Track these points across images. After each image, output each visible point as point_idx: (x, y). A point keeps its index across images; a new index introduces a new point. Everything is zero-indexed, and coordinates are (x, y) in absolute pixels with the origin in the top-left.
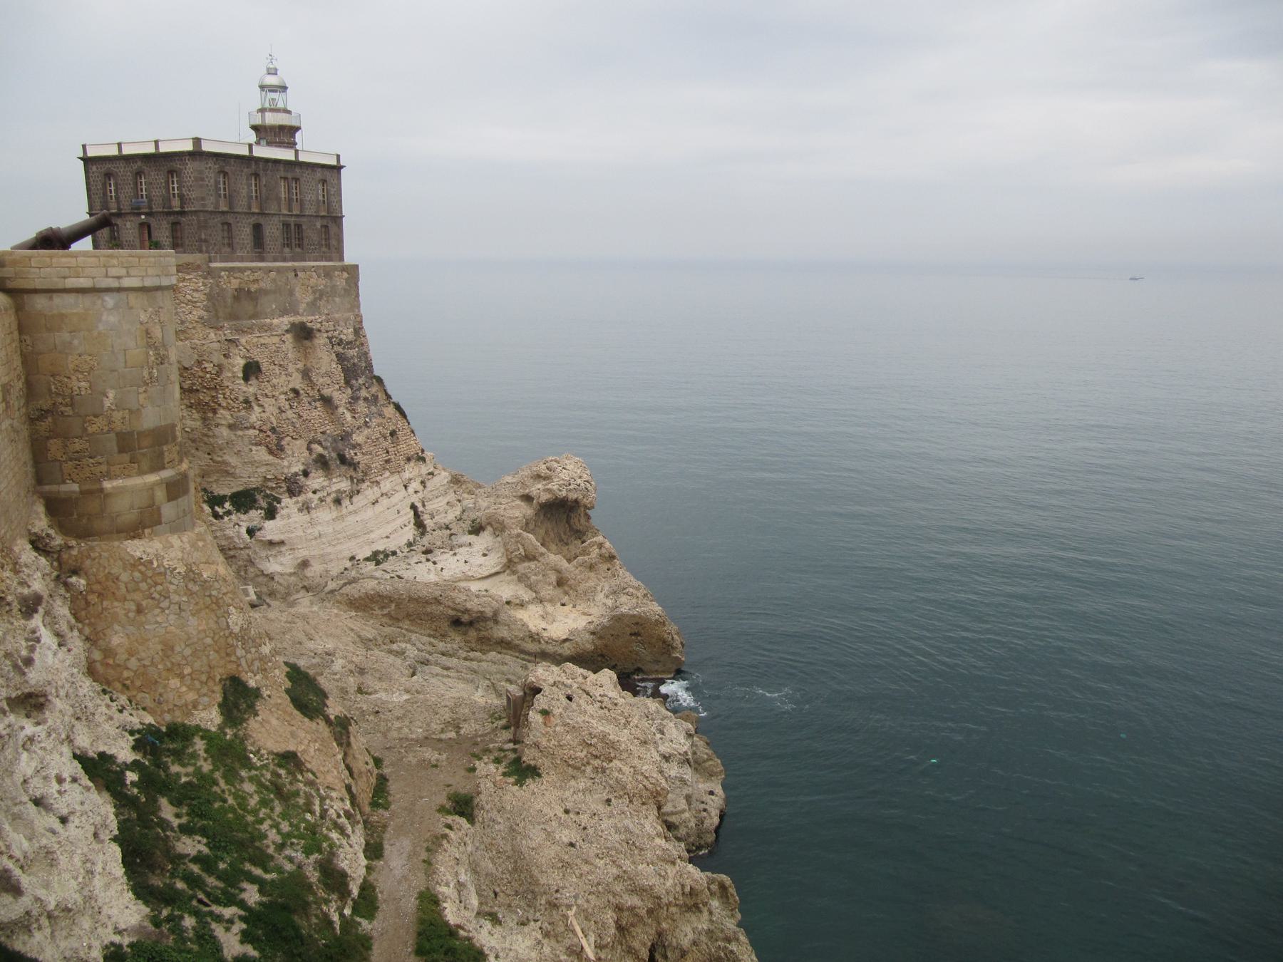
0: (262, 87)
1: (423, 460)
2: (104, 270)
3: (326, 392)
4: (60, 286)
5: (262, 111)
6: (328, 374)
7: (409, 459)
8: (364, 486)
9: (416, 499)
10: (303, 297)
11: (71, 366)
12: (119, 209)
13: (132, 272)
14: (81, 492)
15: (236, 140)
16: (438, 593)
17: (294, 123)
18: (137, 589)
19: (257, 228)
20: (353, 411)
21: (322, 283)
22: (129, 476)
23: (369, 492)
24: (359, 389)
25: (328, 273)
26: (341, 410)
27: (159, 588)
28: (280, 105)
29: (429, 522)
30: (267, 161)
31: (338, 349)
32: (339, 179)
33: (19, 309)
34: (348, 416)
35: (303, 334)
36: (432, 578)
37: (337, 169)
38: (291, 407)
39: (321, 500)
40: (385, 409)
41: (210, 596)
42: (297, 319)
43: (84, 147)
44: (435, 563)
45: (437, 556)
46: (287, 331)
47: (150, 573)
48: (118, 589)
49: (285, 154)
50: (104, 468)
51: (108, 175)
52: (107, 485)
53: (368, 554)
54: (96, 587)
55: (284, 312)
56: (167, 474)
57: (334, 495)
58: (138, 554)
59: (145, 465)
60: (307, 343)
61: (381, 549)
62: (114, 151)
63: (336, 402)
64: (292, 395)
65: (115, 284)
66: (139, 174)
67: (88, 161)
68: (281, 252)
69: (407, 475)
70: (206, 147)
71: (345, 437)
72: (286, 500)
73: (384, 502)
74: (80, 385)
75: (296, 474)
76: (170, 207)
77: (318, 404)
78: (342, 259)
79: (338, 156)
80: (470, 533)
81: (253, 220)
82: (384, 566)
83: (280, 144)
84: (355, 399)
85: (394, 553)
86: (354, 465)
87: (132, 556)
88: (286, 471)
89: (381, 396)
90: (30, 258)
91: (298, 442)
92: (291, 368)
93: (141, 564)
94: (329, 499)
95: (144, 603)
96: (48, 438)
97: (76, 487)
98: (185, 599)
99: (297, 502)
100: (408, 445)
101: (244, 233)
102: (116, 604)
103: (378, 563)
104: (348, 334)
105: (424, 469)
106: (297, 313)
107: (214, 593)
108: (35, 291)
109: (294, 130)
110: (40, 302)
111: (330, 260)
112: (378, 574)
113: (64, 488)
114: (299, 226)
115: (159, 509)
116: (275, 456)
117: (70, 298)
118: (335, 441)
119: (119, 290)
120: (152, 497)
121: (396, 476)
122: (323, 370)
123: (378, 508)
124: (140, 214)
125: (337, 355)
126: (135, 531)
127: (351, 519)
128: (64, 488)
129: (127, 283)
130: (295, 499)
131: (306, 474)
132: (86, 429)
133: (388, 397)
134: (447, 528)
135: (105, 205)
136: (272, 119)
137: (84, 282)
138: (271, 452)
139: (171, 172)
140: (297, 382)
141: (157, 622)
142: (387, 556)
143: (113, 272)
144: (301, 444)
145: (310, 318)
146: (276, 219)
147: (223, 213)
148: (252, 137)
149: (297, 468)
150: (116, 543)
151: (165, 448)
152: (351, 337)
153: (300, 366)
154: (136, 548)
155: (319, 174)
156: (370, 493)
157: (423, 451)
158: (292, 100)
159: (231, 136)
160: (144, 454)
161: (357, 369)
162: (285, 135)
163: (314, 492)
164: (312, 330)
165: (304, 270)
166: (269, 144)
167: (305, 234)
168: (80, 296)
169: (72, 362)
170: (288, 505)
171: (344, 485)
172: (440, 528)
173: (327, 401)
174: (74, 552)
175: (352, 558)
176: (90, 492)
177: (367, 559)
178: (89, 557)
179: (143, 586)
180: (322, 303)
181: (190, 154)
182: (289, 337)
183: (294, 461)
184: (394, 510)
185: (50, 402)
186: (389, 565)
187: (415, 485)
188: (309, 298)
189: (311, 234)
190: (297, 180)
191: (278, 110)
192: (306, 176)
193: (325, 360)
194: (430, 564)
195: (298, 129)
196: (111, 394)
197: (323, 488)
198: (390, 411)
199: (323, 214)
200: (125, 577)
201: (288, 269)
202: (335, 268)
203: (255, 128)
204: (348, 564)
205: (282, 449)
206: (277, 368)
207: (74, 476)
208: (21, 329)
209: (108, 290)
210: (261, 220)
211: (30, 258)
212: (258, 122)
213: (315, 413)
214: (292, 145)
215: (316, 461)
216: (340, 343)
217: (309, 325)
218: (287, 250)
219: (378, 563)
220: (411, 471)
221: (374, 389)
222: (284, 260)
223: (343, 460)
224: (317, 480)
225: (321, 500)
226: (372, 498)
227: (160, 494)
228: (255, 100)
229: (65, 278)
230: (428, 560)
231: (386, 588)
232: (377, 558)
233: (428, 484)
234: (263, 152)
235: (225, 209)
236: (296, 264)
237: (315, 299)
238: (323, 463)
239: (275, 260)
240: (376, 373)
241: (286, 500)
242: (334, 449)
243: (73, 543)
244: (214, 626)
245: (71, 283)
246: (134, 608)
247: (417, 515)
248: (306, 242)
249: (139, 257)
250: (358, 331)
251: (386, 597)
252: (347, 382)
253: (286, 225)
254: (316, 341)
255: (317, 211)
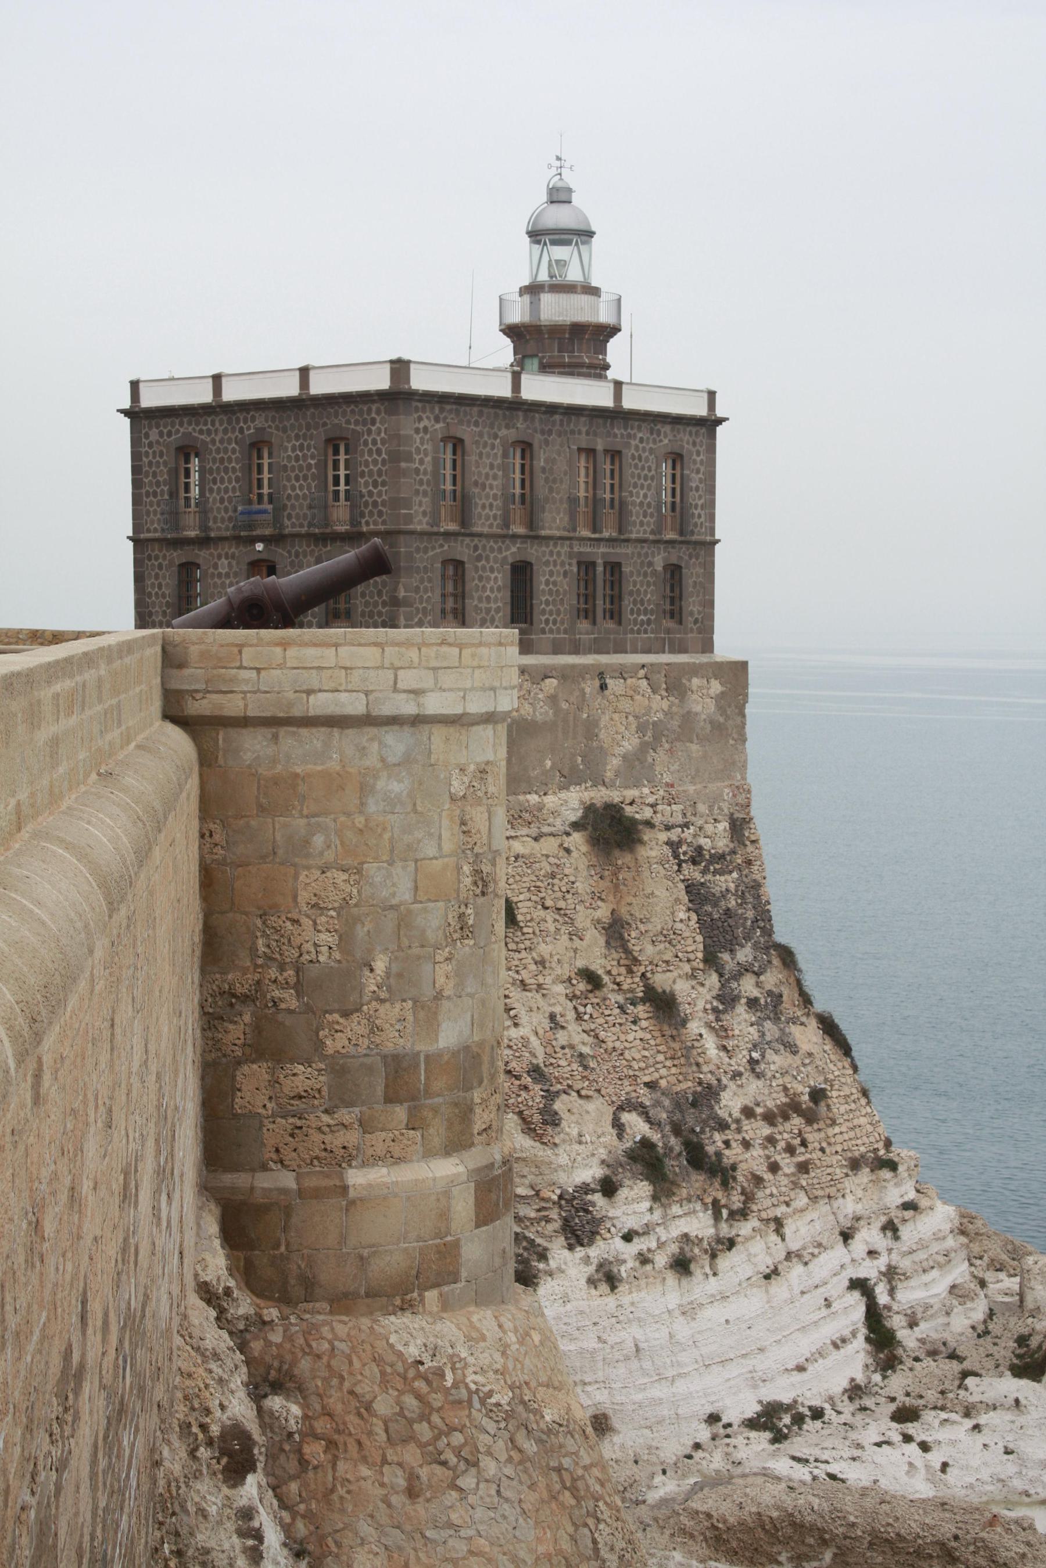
0: (536, 235)
1: (892, 1166)
2: (390, 675)
3: (661, 980)
4: (297, 712)
5: (533, 290)
6: (669, 936)
7: (855, 1165)
8: (745, 1228)
9: (869, 1270)
10: (620, 740)
11: (304, 896)
12: (204, 527)
13: (448, 679)
14: (301, 1193)
15: (465, 364)
16: (948, 1529)
17: (604, 316)
18: (410, 1438)
19: (521, 574)
20: (722, 1032)
21: (660, 704)
22: (399, 1160)
23: (757, 1246)
24: (737, 976)
25: (674, 684)
26: (695, 1027)
27: (457, 1439)
28: (574, 274)
29: (908, 1339)
30: (552, 409)
31: (692, 872)
32: (712, 449)
33: (206, 760)
34: (710, 1044)
35: (612, 832)
36: (921, 1488)
37: (710, 424)
38: (579, 1017)
39: (644, 1259)
40: (795, 1030)
41: (559, 1470)
42: (601, 795)
43: (135, 385)
44: (925, 1447)
45: (930, 1426)
46: (576, 826)
47: (437, 1400)
48: (370, 1433)
49: (591, 394)
50: (352, 1137)
51: (185, 451)
52: (357, 1178)
53: (752, 1409)
54: (322, 1425)
55: (570, 778)
56: (476, 1157)
57: (674, 1248)
58: (413, 1351)
59: (437, 1132)
60: (624, 859)
61: (786, 1398)
62: (204, 396)
63: (685, 1009)
64: (582, 986)
65: (409, 708)
66: (257, 446)
67: (136, 415)
68: (571, 630)
69: (849, 1206)
70: (420, 381)
71: (710, 1093)
72: (559, 1254)
73: (796, 1272)
74: (319, 942)
75: (585, 1189)
76: (327, 522)
77: (641, 1011)
78: (708, 646)
79: (712, 395)
80: (1020, 1371)
81: (512, 552)
82: (798, 1445)
83: (572, 369)
84: (727, 1000)
85: (817, 1414)
86: (721, 1172)
87: (400, 1355)
88: (562, 1178)
89: (789, 994)
90: (240, 647)
91: (591, 1106)
92: (583, 918)
93: (419, 1376)
94: (661, 1260)
95: (424, 1473)
96: (239, 1063)
97: (288, 1180)
98: (509, 1471)
99: (587, 1260)
100: (853, 1127)
101: (491, 585)
102: (365, 1471)
103: (779, 1438)
104: (716, 837)
105: (898, 1191)
106: (599, 781)
107: (566, 1462)
108: (244, 722)
109: (603, 334)
110: (253, 745)
111: (681, 648)
112: (782, 1466)
113: (264, 1181)
114: (614, 568)
115: (456, 1244)
116: (539, 1138)
117: (315, 738)
118: (677, 1105)
119: (418, 721)
120: (444, 1215)
121: (823, 1207)
122: (656, 925)
123: (779, 1289)
124: (253, 540)
125: (691, 888)
126: (401, 1294)
127: (714, 1314)
128: (264, 1181)
129: (434, 704)
130: (580, 1252)
131: (609, 1188)
132: (320, 1044)
133: (806, 1000)
134: (953, 1356)
135: (174, 517)
136: (555, 309)
137: (353, 705)
138: (529, 1128)
139: (333, 443)
140: (596, 955)
141: (450, 1525)
142: (799, 1420)
143: (408, 679)
144: (598, 1111)
145: (631, 793)
146: (564, 549)
147: (447, 535)
148: (503, 352)
149: (590, 1173)
150: (365, 1322)
151: (477, 1095)
152: (723, 844)
153: (603, 912)
154: (409, 1334)
155: (666, 439)
156: (757, 1250)
157: (888, 1144)
158: (605, 265)
159: (467, 352)
160: (435, 1110)
161: (732, 924)
162: (581, 345)
163: (628, 1238)
164: (634, 822)
165: (622, 673)
166: (546, 368)
167: (628, 587)
168: (336, 731)
169: (309, 884)
170: (568, 1267)
171: (699, 1224)
172: (933, 1353)
173: (664, 1006)
174: (276, 1337)
175: (713, 1419)
176: (317, 1194)
177: (752, 1424)
178: (308, 1350)
179: (423, 1430)
180: (659, 756)
181: (381, 396)
182: (577, 839)
183: (578, 1157)
184: (816, 1298)
185: (252, 977)
186: (807, 1441)
187: (869, 1236)
188: (629, 744)
189: (642, 588)
190: (615, 455)
191: (569, 288)
192: (637, 444)
193: (660, 897)
194: (913, 1448)
195: (613, 330)
196: (380, 965)
197: (647, 1230)
198: (808, 1037)
199: (671, 536)
200: (384, 1406)
201: (582, 672)
202: (694, 670)
203: (512, 331)
204: (704, 1434)
205: (552, 1120)
206: (549, 916)
207: (288, 1155)
208: (210, 806)
209: (394, 721)
210: (533, 552)
211: (240, 647)
212: (517, 316)
213: (634, 1034)
214: (598, 370)
215: (632, 1156)
216: (697, 856)
217: (629, 810)
218: (584, 625)
219: (779, 1438)
220: (859, 1195)
221: (772, 978)
222: (576, 651)
223: (697, 1157)
224: (633, 1204)
225: (644, 1259)
226: (765, 1263)
227: (463, 1206)
228: (520, 263)
229: (309, 692)
230: (907, 1439)
231: (810, 1504)
232: (773, 1421)
233: (905, 1232)
234: (543, 388)
235: (453, 527)
236: (604, 659)
237: (644, 747)
238: (646, 1160)
239: (557, 650)
240: (781, 936)
241: (559, 1254)
242: (677, 1131)
243: (272, 1313)
244: (566, 1545)
245: (320, 704)
246: (402, 1482)
247: (874, 1317)
248: (627, 603)
249: (461, 647)
250: (739, 827)
251: (813, 1528)
252: (710, 960)
253: (587, 566)
254: (643, 852)
255: (658, 530)
